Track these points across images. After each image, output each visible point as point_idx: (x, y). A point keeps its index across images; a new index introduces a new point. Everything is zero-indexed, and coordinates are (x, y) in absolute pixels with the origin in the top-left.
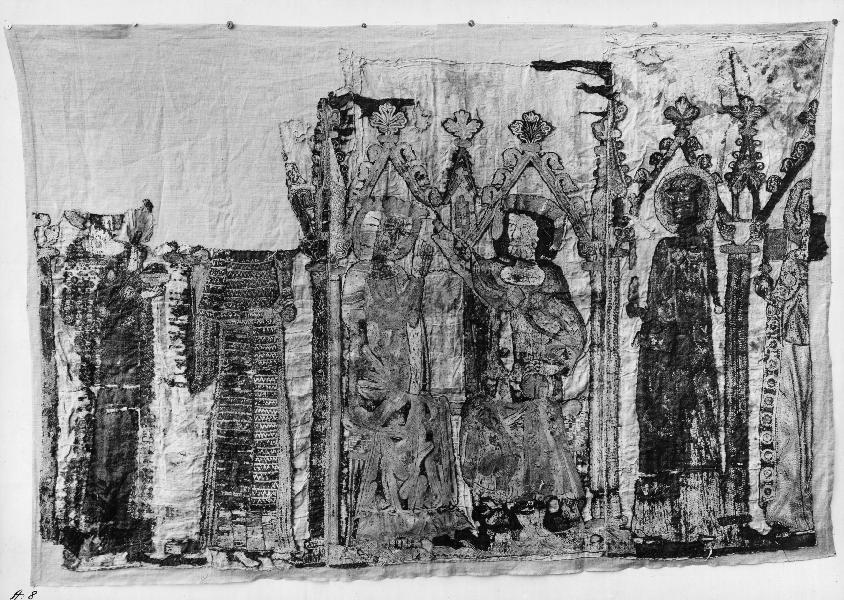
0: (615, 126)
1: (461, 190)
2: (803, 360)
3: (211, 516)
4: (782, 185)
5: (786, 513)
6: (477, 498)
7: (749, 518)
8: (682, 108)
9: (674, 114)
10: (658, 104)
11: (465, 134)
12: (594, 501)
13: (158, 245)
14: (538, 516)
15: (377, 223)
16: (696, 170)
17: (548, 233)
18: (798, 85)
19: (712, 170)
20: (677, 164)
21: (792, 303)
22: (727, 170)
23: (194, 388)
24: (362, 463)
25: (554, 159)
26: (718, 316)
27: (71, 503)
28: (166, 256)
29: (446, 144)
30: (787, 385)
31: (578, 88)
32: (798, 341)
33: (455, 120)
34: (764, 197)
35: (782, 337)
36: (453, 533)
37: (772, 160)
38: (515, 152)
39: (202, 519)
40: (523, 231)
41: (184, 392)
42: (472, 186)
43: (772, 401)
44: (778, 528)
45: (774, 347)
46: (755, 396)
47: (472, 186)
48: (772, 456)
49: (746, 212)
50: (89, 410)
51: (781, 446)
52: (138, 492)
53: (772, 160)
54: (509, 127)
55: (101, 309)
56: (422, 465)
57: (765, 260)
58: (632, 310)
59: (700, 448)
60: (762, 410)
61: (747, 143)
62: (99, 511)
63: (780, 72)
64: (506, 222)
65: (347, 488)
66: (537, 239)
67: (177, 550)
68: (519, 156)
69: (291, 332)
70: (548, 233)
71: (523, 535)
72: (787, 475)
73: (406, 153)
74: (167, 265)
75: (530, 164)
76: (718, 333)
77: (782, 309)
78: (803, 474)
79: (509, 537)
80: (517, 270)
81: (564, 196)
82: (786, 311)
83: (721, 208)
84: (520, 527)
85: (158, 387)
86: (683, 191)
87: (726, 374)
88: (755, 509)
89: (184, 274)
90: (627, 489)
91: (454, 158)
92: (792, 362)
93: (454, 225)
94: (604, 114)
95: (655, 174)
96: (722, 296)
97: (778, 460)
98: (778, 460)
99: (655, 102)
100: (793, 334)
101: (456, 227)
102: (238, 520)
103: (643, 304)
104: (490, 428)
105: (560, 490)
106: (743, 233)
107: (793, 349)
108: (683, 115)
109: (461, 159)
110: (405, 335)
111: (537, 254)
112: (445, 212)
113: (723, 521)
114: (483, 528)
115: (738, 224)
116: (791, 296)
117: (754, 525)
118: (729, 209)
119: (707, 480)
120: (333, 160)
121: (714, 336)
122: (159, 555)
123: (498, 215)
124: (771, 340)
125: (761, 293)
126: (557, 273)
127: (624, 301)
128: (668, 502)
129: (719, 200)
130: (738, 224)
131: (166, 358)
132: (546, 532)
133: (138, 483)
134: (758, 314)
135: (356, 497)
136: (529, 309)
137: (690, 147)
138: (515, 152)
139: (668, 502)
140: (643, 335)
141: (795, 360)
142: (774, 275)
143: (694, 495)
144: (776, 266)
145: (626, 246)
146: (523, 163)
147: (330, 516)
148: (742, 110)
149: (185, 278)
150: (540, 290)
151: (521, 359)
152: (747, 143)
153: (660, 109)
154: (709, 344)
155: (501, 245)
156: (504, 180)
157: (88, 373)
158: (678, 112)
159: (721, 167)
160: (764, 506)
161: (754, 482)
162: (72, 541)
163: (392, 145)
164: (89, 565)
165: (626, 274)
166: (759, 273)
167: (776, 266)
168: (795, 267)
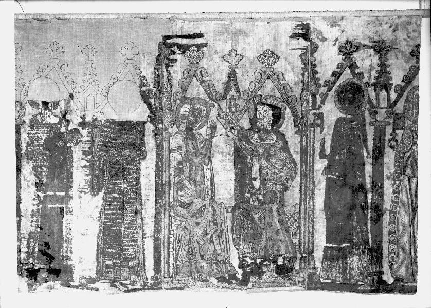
0: (312, 56)
1: (233, 93)
2: (414, 186)
3: (102, 263)
4: (400, 91)
5: (402, 271)
6: (241, 256)
7: (382, 273)
8: (348, 46)
9: (344, 50)
10: (335, 44)
11: (234, 62)
12: (301, 259)
13: (75, 120)
14: (273, 267)
15: (188, 110)
16: (356, 81)
17: (277, 117)
18: (409, 35)
19: (364, 80)
20: (347, 75)
21: (408, 154)
22: (373, 81)
23: (95, 192)
24: (178, 235)
25: (281, 75)
26: (369, 160)
27: (30, 253)
28: (80, 124)
29: (225, 68)
30: (405, 199)
31: (291, 37)
32: (412, 175)
33: (229, 55)
34: (394, 96)
35: (403, 173)
36: (227, 275)
37: (397, 77)
38: (260, 72)
39: (98, 266)
40: (265, 114)
41: (89, 195)
42: (238, 91)
43: (396, 208)
44: (397, 279)
45: (398, 178)
46: (387, 205)
47: (238, 91)
48: (395, 237)
49: (384, 104)
50: (38, 206)
51: (400, 232)
52: (65, 249)
53: (397, 77)
54: (257, 58)
55: (46, 153)
56: (211, 237)
57: (394, 130)
58: (323, 155)
59: (358, 233)
60: (391, 212)
61: (383, 65)
62: (44, 261)
63: (399, 27)
64: (256, 110)
65: (173, 248)
66: (272, 118)
67: (84, 281)
68: (263, 74)
69: (143, 164)
70: (277, 117)
71: (264, 277)
72: (403, 249)
73: (203, 73)
74: (80, 129)
75: (268, 78)
76: (369, 169)
77: (404, 157)
78: (412, 250)
79: (257, 278)
80: (262, 135)
81: (285, 89)
82: (405, 159)
83: (370, 102)
84: (264, 273)
85: (74, 192)
86: (349, 91)
87: (372, 192)
88: (386, 268)
89: (89, 133)
90: (319, 254)
91: (229, 76)
92: (408, 186)
93: (228, 111)
94: (306, 49)
95: (334, 83)
96: (371, 148)
97: (398, 240)
98: (398, 240)
99: (334, 43)
100: (409, 171)
101: (229, 112)
102: (116, 265)
103: (328, 151)
104: (247, 220)
105: (284, 253)
106: (382, 115)
107: (409, 180)
108: (348, 49)
109: (232, 76)
110: (202, 170)
111: (272, 127)
112: (224, 104)
113: (370, 274)
114: (244, 274)
115: (379, 110)
116: (408, 150)
117: (385, 277)
118: (374, 101)
119: (362, 251)
120: (165, 74)
121: (366, 171)
122: (76, 283)
123: (252, 106)
124: (397, 174)
125: (392, 147)
126: (282, 136)
127: (318, 151)
128: (340, 261)
129: (369, 97)
130: (379, 110)
131: (80, 176)
132: (276, 275)
133: (65, 245)
134: (390, 158)
135: (178, 254)
136: (268, 156)
137: (353, 67)
138: (260, 72)
139: (340, 261)
140: (328, 169)
141: (410, 185)
142: (399, 138)
143: (355, 258)
144: (400, 132)
145: (319, 122)
146: (265, 77)
147: (164, 264)
148: (381, 48)
149: (89, 135)
150: (273, 145)
151: (264, 183)
152: (383, 65)
153: (336, 48)
154: (363, 176)
155: (253, 120)
156: (255, 87)
157: (39, 185)
158: (346, 49)
159: (369, 79)
160: (391, 266)
161: (385, 253)
162: (32, 274)
163: (195, 69)
164: (42, 289)
165: (318, 136)
166: (391, 137)
167: (400, 132)
168: (411, 134)
